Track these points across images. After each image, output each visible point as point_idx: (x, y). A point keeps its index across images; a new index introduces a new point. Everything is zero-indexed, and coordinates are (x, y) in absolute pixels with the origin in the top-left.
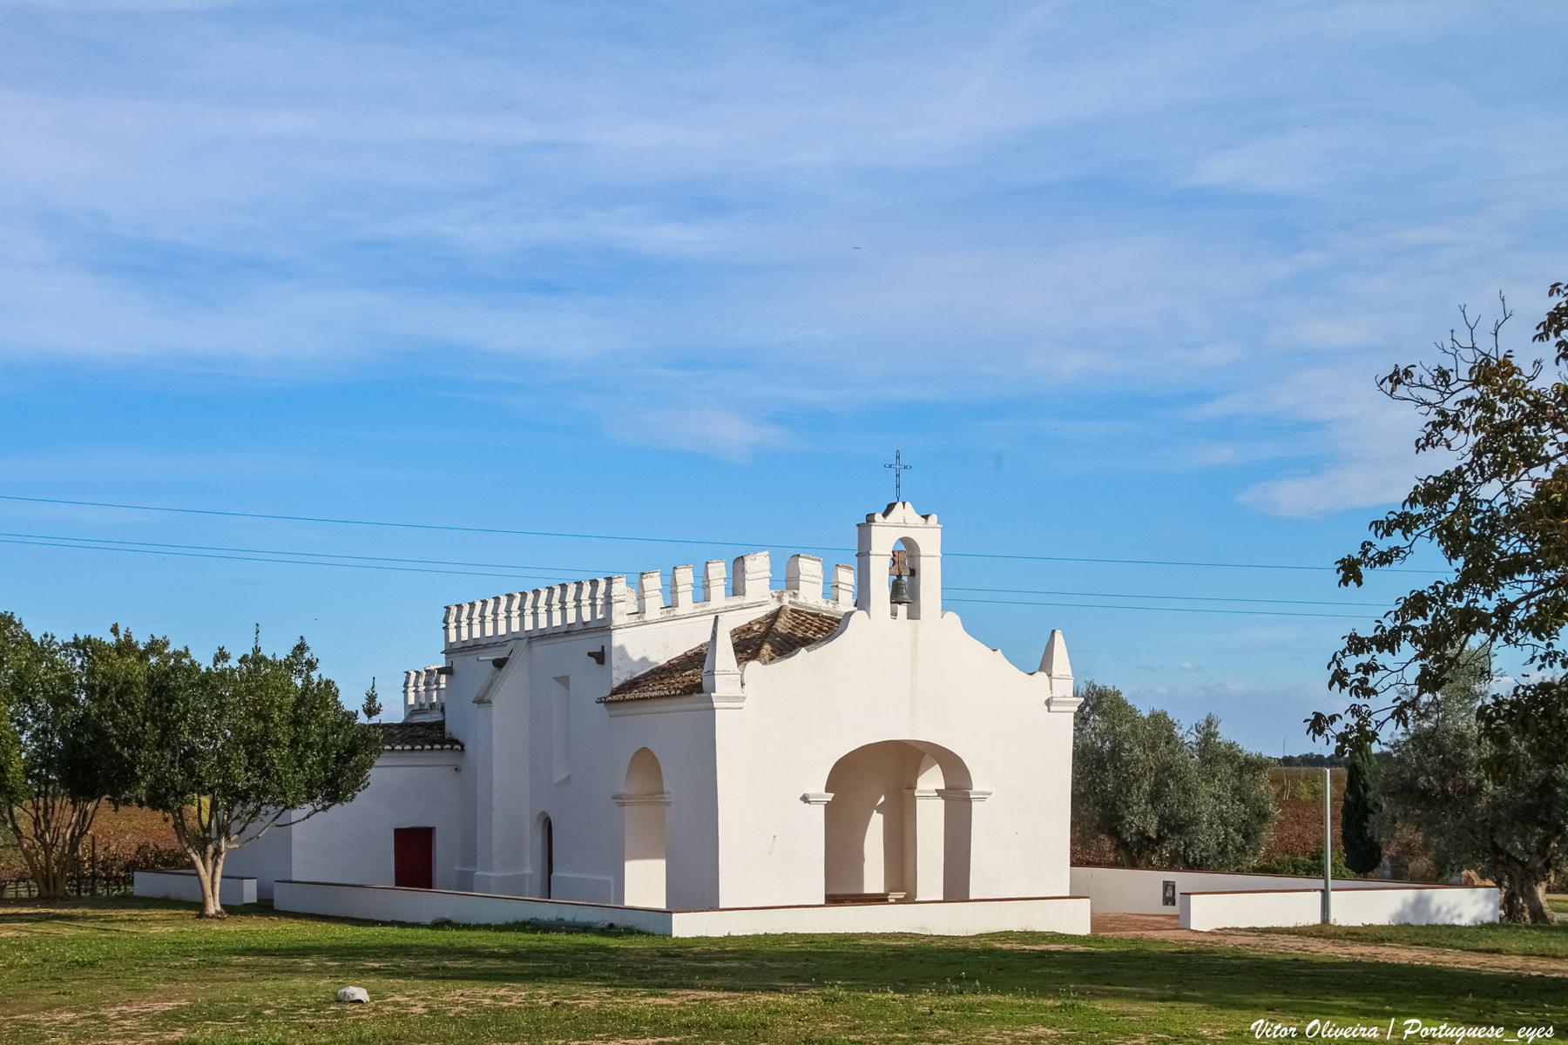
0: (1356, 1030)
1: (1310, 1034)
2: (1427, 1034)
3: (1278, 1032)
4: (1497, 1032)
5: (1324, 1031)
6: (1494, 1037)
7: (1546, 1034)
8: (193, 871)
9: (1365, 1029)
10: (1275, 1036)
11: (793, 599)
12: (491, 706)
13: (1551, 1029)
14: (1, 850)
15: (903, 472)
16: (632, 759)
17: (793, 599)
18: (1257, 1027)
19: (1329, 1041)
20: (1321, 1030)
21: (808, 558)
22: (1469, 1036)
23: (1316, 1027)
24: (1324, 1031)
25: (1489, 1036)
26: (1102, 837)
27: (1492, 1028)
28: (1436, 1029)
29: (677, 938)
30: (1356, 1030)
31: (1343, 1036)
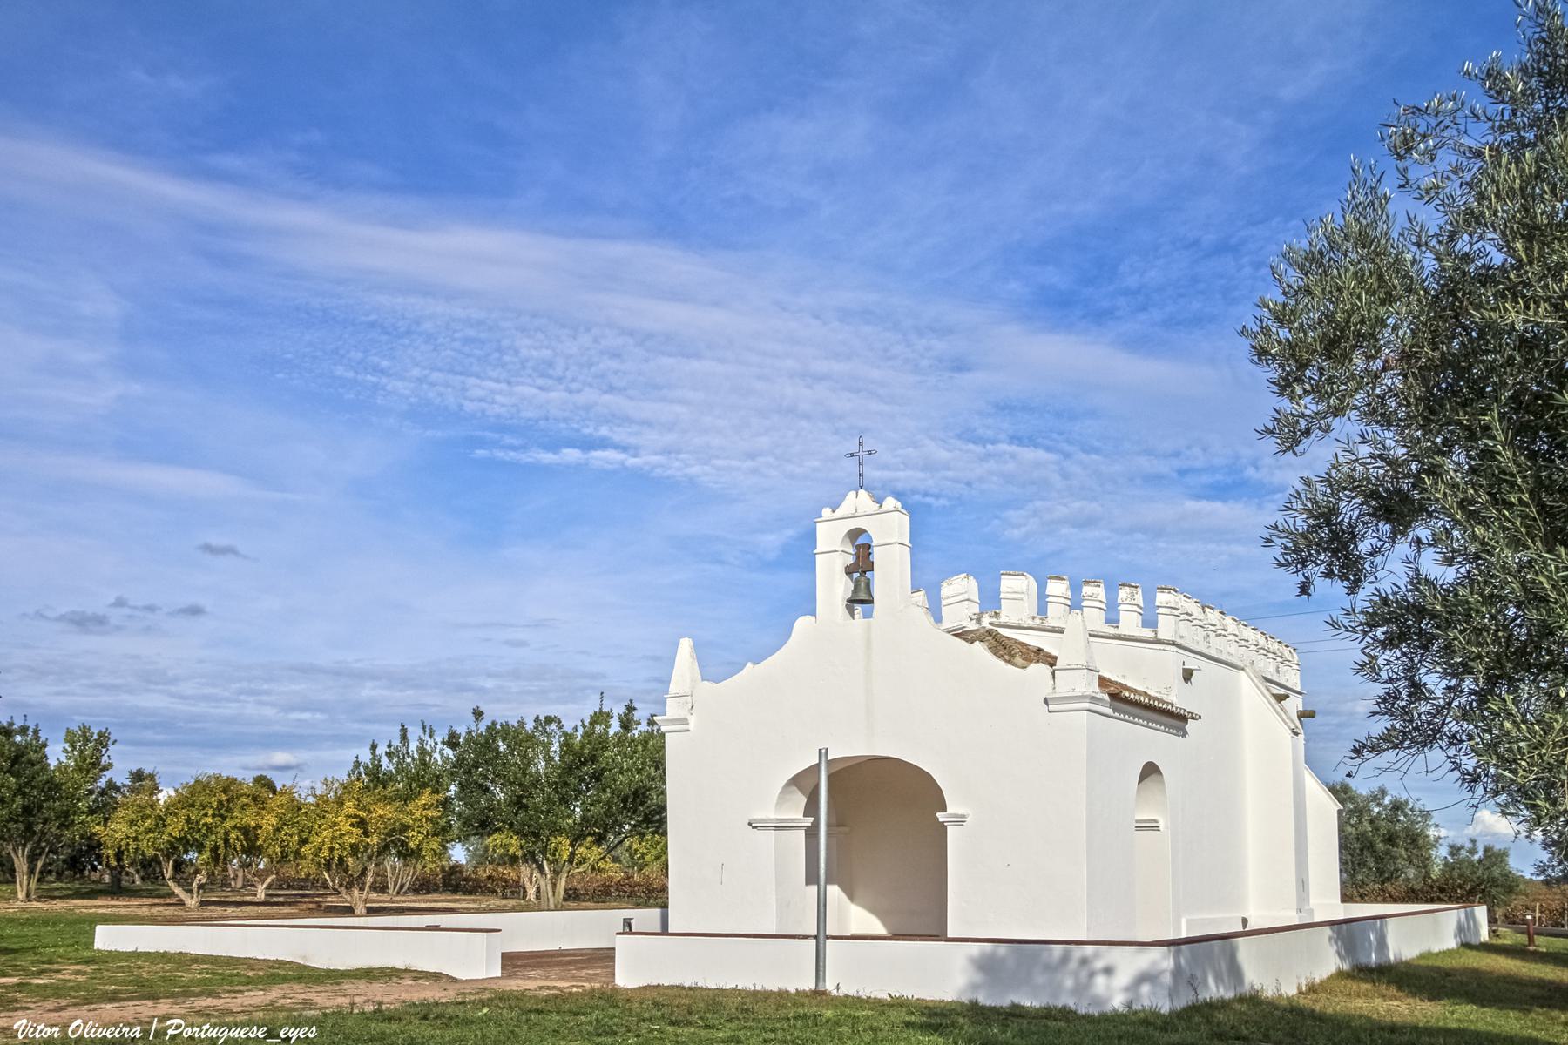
0: (119, 1030)
1: (73, 1033)
2: (189, 1034)
3: (41, 1032)
4: (260, 1032)
5: (86, 1031)
6: (105, 1036)
7: (309, 1034)
8: (174, 901)
9: (128, 1029)
10: (38, 1036)
11: (994, 620)
12: (1162, 782)
13: (314, 1029)
14: (4, 888)
15: (855, 448)
16: (781, 792)
17: (994, 620)
18: (20, 1026)
19: (92, 1040)
20: (83, 1030)
21: (1010, 574)
22: (232, 1035)
23: (78, 1026)
24: (86, 1031)
25: (252, 1036)
26: (311, 800)
27: (255, 1028)
28: (198, 1029)
29: (99, 951)
30: (119, 1030)
31: (105, 1036)
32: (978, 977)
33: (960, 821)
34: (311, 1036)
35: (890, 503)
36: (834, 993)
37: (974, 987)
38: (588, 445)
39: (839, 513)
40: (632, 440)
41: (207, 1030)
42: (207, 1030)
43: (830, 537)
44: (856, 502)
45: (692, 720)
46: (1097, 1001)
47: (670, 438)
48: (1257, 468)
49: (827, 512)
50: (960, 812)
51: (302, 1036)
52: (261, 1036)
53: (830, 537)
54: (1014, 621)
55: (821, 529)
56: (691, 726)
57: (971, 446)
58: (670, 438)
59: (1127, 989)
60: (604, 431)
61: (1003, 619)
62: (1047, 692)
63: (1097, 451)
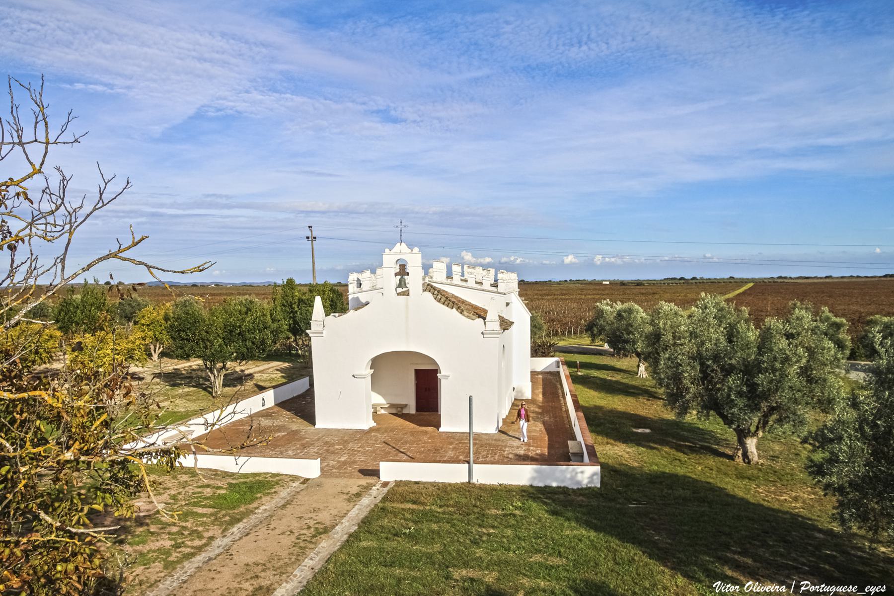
4: (854, 589)
7: (848, 590)
11: (430, 280)
17: (430, 280)
18: (717, 585)
28: (818, 587)
30: (773, 587)
32: (535, 475)
33: (447, 377)
34: (883, 591)
35: (416, 250)
36: (476, 483)
37: (534, 478)
38: (87, 83)
39: (393, 251)
40: (111, 82)
41: (823, 588)
42: (823, 588)
43: (390, 261)
44: (401, 249)
45: (324, 332)
46: (579, 483)
47: (129, 83)
48: (396, 111)
49: (387, 251)
50: (447, 374)
51: (878, 591)
52: (854, 591)
53: (390, 261)
54: (439, 280)
55: (385, 257)
56: (324, 335)
57: (274, 94)
58: (129, 83)
59: (589, 478)
60: (97, 76)
61: (434, 279)
62: (483, 329)
63: (331, 100)
